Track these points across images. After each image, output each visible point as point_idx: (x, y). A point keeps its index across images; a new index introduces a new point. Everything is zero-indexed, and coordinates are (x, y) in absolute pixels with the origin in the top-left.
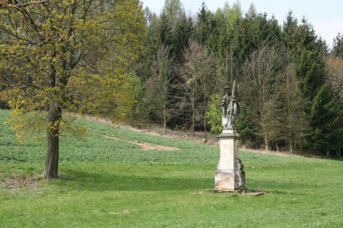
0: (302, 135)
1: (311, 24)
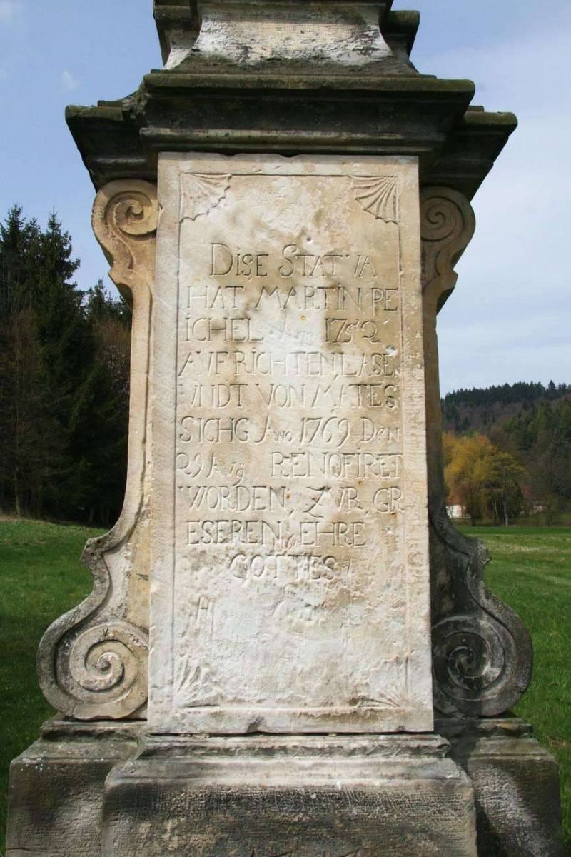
0: (47, 472)
1: (69, 235)
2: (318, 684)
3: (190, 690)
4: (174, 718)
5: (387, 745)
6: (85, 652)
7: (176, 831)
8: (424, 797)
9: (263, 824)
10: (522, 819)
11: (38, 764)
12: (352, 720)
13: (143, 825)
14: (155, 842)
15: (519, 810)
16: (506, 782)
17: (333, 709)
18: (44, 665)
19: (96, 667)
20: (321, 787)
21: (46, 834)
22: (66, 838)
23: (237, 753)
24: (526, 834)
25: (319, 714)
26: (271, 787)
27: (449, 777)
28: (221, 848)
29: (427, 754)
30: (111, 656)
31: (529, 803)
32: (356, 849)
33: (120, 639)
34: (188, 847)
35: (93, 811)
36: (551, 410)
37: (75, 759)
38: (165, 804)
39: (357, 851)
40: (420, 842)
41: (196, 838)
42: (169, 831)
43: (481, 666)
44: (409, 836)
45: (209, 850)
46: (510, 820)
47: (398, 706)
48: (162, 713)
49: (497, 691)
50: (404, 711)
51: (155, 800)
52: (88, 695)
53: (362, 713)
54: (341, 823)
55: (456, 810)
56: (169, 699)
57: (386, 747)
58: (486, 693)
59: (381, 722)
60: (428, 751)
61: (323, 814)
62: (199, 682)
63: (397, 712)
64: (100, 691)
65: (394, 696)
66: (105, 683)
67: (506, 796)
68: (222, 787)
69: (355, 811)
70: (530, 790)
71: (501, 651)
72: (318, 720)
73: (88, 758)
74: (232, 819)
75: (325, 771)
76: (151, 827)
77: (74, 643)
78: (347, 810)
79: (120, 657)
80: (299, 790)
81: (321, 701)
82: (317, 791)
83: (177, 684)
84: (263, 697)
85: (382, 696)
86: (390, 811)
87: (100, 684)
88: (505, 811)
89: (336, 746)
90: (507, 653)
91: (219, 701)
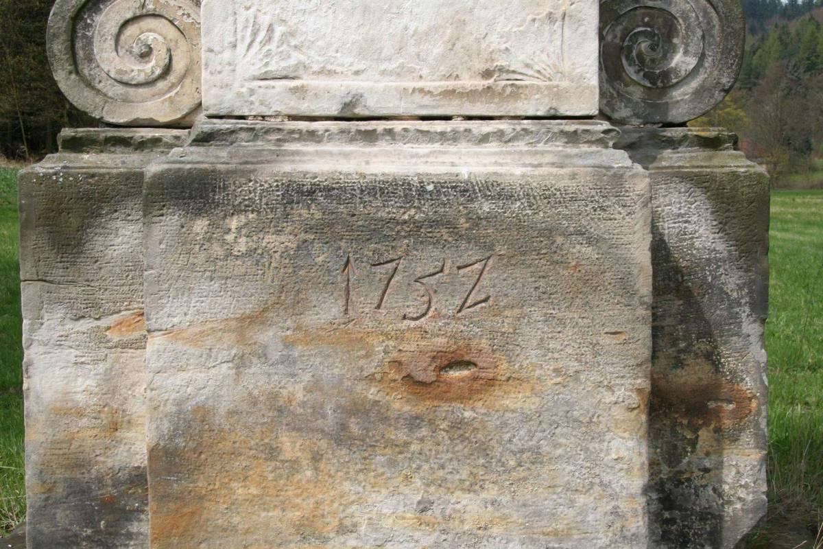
2: (438, 50)
3: (261, 56)
4: (239, 95)
5: (533, 129)
6: (115, 30)
7: (244, 231)
8: (582, 189)
9: (360, 223)
10: (714, 248)
11: (55, 174)
12: (489, 103)
13: (199, 222)
14: (215, 244)
15: (712, 236)
16: (696, 201)
17: (459, 83)
18: (57, 47)
19: (131, 52)
20: (440, 175)
21: (74, 263)
22: (100, 268)
23: (325, 139)
24: (719, 267)
25: (440, 90)
26: (372, 174)
27: (616, 166)
28: (305, 252)
29: (588, 142)
30: (152, 37)
31: (727, 227)
32: (487, 254)
33: (164, 14)
34: (260, 251)
35: (135, 235)
36: (788, 34)
37: (107, 168)
38: (228, 194)
39: (489, 258)
40: (574, 247)
41: (270, 240)
42: (233, 230)
43: (669, 55)
44: (559, 240)
45: (289, 255)
46: (698, 249)
47: (550, 80)
48: (222, 88)
49: (690, 91)
50: (557, 86)
51: (214, 191)
52: (122, 92)
53: (499, 88)
54: (467, 222)
55: (625, 206)
56: (231, 68)
57: (532, 132)
58: (674, 93)
59: (526, 102)
60: (589, 137)
61: (443, 210)
62: (273, 46)
63: (548, 88)
64: (138, 85)
65: (544, 66)
66: (146, 74)
67: (694, 218)
68: (305, 174)
69: (486, 207)
70: (728, 211)
71: (699, 33)
72: (438, 98)
73: (126, 168)
74: (318, 215)
75: (448, 159)
76: (210, 225)
77: (99, 18)
78: (476, 205)
79: (165, 38)
80: (410, 178)
81: (443, 73)
82: (435, 180)
83: (241, 48)
84: (361, 67)
85: (527, 66)
86: (535, 206)
87: (139, 75)
88: (692, 238)
89: (462, 129)
90: (707, 37)
91: (301, 72)
